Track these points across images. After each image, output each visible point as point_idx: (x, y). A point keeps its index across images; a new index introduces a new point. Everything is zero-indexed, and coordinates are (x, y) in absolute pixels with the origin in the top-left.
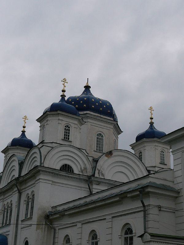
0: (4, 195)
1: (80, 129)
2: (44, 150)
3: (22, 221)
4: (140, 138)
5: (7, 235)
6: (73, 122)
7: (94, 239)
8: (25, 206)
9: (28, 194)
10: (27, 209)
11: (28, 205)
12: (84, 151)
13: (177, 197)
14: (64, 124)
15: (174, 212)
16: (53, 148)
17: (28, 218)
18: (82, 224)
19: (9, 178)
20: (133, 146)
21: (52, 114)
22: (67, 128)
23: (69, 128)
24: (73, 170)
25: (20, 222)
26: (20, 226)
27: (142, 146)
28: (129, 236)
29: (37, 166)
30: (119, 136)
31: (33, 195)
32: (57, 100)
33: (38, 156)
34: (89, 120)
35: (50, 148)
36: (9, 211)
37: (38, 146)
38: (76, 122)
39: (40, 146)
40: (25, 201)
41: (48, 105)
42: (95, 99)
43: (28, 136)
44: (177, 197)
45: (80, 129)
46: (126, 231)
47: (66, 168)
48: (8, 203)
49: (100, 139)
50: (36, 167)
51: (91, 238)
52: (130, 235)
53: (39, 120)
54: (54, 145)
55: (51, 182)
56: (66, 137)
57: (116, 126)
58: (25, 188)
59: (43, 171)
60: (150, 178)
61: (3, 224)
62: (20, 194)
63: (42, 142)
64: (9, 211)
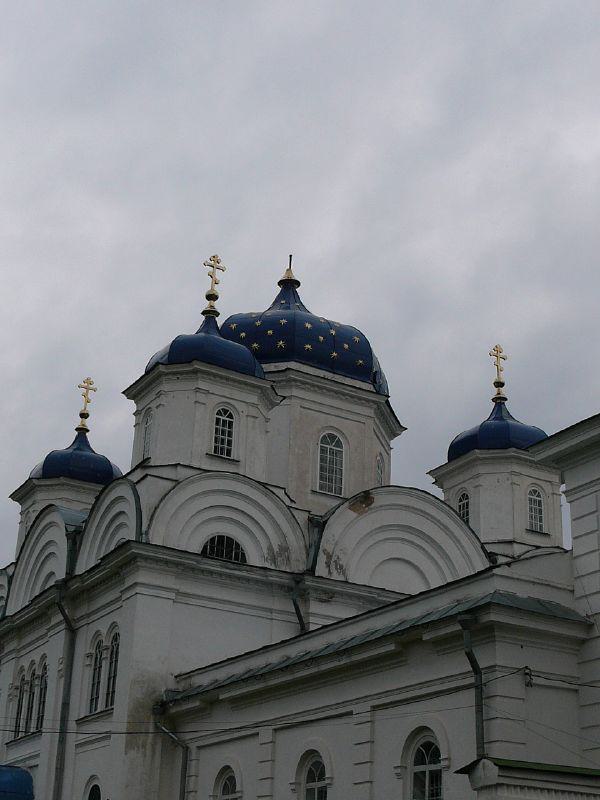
0: (20, 638)
1: (267, 420)
2: (149, 491)
3: (80, 722)
4: (461, 448)
5: (31, 767)
6: (243, 399)
7: (314, 781)
8: (89, 672)
9: (98, 633)
10: (96, 685)
11: (97, 670)
12: (280, 493)
13: (583, 641)
14: (213, 403)
15: (576, 691)
16: (177, 482)
17: (99, 710)
18: (275, 730)
19: (35, 583)
20: (439, 476)
21: (174, 374)
23: (231, 416)
24: (243, 555)
25: (72, 725)
26: (72, 739)
27: (467, 475)
28: (428, 768)
29: (129, 541)
30: (393, 443)
31: (116, 638)
32: (190, 325)
33: (130, 509)
34: (295, 392)
35: (170, 485)
36: (37, 690)
37: (129, 477)
38: (254, 399)
39: (135, 478)
40: (89, 656)
41: (160, 344)
42: (315, 321)
43: (98, 444)
44: (583, 641)
45: (267, 420)
46: (419, 751)
47: (223, 549)
48: (33, 663)
49: (332, 452)
50: (125, 545)
51: (304, 776)
52: (433, 767)
53: (133, 392)
54: (182, 473)
55: (173, 596)
56: (222, 449)
57: (385, 409)
58: (89, 615)
59: (146, 558)
60: (495, 579)
61: (17, 732)
62: (72, 632)
63: (143, 464)
64: (37, 690)
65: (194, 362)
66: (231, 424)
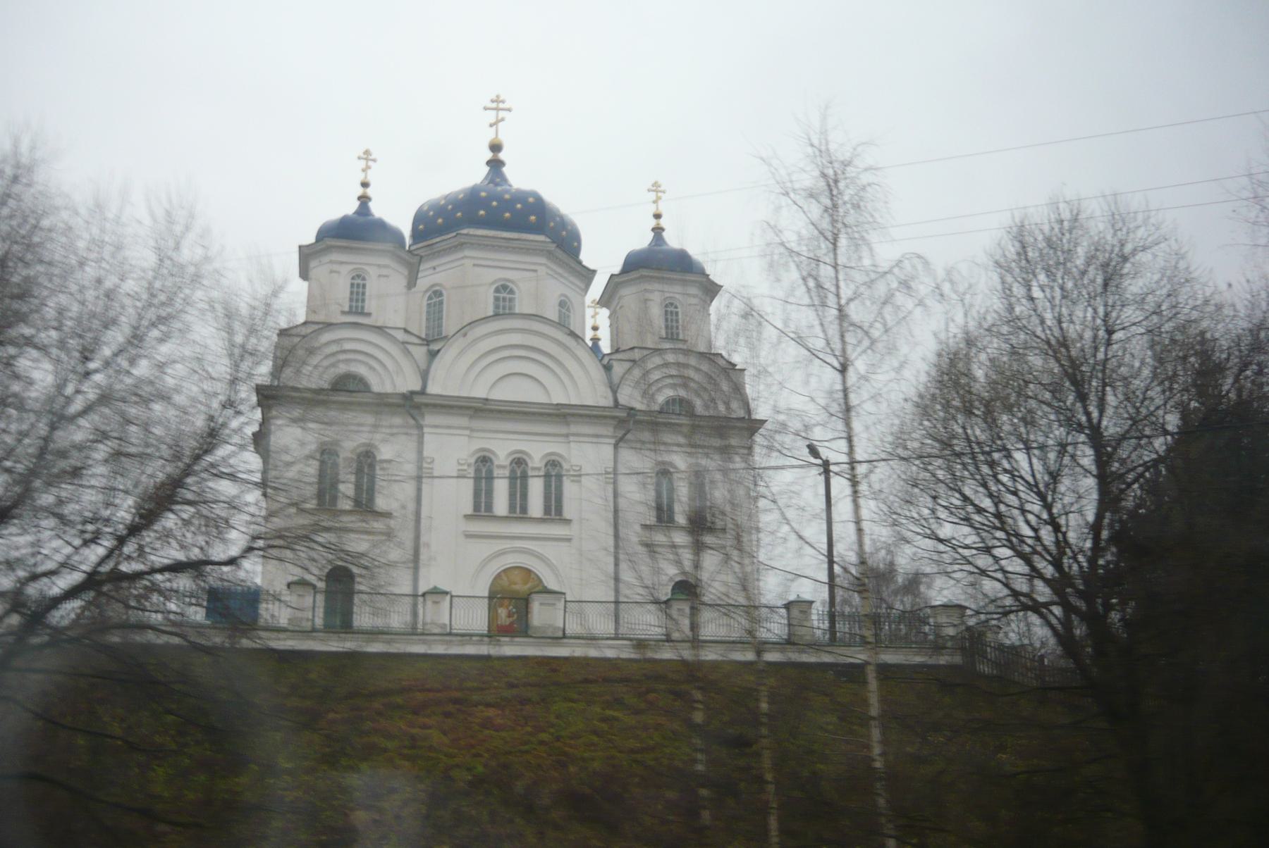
16: (634, 361)
22: (505, 295)
65: (641, 270)
66: (364, 286)
